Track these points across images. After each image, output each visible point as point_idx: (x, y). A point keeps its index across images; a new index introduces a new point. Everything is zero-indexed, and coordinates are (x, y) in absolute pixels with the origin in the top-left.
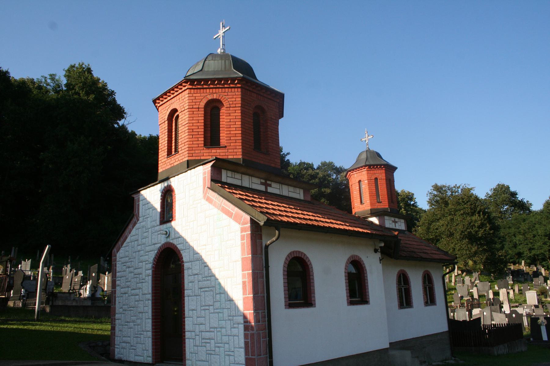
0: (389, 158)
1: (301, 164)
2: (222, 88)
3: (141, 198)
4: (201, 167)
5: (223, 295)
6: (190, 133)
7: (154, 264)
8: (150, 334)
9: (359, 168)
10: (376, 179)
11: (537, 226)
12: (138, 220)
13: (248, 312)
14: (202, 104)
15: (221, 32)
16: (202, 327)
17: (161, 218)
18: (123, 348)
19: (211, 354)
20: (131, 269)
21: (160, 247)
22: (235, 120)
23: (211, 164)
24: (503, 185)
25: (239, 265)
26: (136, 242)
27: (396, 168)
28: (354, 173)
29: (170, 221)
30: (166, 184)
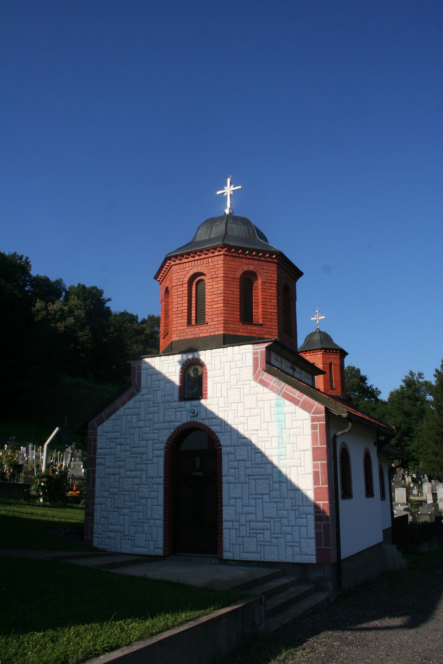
0: (339, 341)
1: (124, 314)
2: (258, 260)
3: (143, 366)
4: (250, 346)
5: (284, 485)
6: (225, 305)
7: (167, 444)
8: (161, 523)
9: (314, 350)
10: (331, 364)
11: (387, 417)
12: (139, 391)
13: (321, 502)
14: (238, 274)
15: (229, 190)
16: (251, 517)
17: (180, 393)
18: (110, 538)
19: (264, 545)
20: (127, 447)
21: (181, 426)
22: (271, 298)
23: (266, 345)
24: (354, 368)
25: (309, 455)
26: (135, 416)
27: (347, 354)
28: (307, 354)
29: (199, 399)
30: (190, 356)
